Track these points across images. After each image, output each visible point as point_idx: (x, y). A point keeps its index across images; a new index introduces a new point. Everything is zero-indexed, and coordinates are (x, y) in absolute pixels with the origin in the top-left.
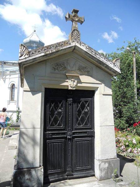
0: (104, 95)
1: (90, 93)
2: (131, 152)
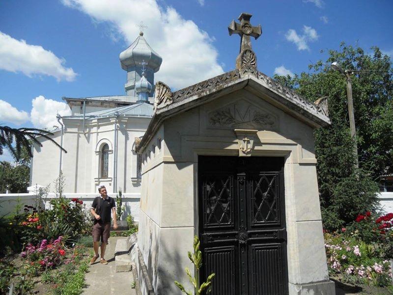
0: (301, 164)
1: (277, 162)
2: (352, 274)
